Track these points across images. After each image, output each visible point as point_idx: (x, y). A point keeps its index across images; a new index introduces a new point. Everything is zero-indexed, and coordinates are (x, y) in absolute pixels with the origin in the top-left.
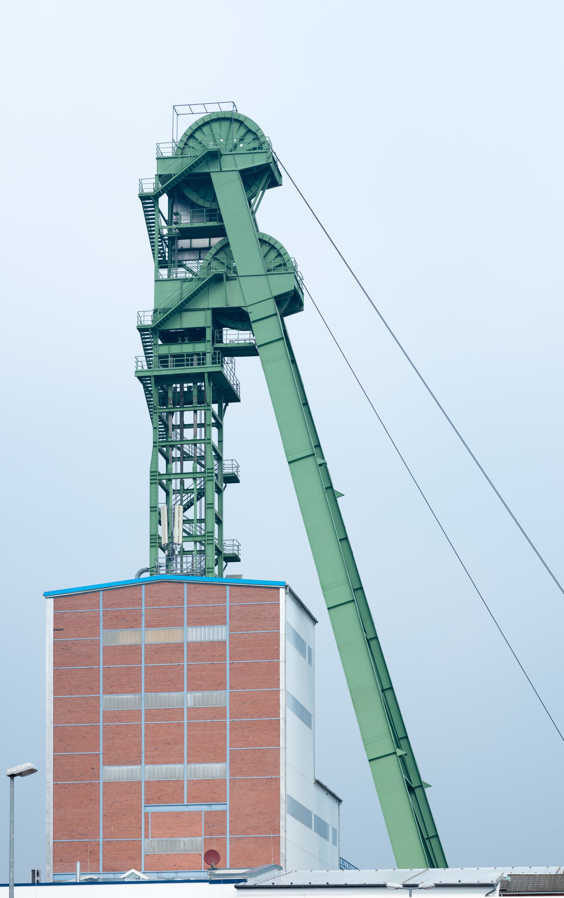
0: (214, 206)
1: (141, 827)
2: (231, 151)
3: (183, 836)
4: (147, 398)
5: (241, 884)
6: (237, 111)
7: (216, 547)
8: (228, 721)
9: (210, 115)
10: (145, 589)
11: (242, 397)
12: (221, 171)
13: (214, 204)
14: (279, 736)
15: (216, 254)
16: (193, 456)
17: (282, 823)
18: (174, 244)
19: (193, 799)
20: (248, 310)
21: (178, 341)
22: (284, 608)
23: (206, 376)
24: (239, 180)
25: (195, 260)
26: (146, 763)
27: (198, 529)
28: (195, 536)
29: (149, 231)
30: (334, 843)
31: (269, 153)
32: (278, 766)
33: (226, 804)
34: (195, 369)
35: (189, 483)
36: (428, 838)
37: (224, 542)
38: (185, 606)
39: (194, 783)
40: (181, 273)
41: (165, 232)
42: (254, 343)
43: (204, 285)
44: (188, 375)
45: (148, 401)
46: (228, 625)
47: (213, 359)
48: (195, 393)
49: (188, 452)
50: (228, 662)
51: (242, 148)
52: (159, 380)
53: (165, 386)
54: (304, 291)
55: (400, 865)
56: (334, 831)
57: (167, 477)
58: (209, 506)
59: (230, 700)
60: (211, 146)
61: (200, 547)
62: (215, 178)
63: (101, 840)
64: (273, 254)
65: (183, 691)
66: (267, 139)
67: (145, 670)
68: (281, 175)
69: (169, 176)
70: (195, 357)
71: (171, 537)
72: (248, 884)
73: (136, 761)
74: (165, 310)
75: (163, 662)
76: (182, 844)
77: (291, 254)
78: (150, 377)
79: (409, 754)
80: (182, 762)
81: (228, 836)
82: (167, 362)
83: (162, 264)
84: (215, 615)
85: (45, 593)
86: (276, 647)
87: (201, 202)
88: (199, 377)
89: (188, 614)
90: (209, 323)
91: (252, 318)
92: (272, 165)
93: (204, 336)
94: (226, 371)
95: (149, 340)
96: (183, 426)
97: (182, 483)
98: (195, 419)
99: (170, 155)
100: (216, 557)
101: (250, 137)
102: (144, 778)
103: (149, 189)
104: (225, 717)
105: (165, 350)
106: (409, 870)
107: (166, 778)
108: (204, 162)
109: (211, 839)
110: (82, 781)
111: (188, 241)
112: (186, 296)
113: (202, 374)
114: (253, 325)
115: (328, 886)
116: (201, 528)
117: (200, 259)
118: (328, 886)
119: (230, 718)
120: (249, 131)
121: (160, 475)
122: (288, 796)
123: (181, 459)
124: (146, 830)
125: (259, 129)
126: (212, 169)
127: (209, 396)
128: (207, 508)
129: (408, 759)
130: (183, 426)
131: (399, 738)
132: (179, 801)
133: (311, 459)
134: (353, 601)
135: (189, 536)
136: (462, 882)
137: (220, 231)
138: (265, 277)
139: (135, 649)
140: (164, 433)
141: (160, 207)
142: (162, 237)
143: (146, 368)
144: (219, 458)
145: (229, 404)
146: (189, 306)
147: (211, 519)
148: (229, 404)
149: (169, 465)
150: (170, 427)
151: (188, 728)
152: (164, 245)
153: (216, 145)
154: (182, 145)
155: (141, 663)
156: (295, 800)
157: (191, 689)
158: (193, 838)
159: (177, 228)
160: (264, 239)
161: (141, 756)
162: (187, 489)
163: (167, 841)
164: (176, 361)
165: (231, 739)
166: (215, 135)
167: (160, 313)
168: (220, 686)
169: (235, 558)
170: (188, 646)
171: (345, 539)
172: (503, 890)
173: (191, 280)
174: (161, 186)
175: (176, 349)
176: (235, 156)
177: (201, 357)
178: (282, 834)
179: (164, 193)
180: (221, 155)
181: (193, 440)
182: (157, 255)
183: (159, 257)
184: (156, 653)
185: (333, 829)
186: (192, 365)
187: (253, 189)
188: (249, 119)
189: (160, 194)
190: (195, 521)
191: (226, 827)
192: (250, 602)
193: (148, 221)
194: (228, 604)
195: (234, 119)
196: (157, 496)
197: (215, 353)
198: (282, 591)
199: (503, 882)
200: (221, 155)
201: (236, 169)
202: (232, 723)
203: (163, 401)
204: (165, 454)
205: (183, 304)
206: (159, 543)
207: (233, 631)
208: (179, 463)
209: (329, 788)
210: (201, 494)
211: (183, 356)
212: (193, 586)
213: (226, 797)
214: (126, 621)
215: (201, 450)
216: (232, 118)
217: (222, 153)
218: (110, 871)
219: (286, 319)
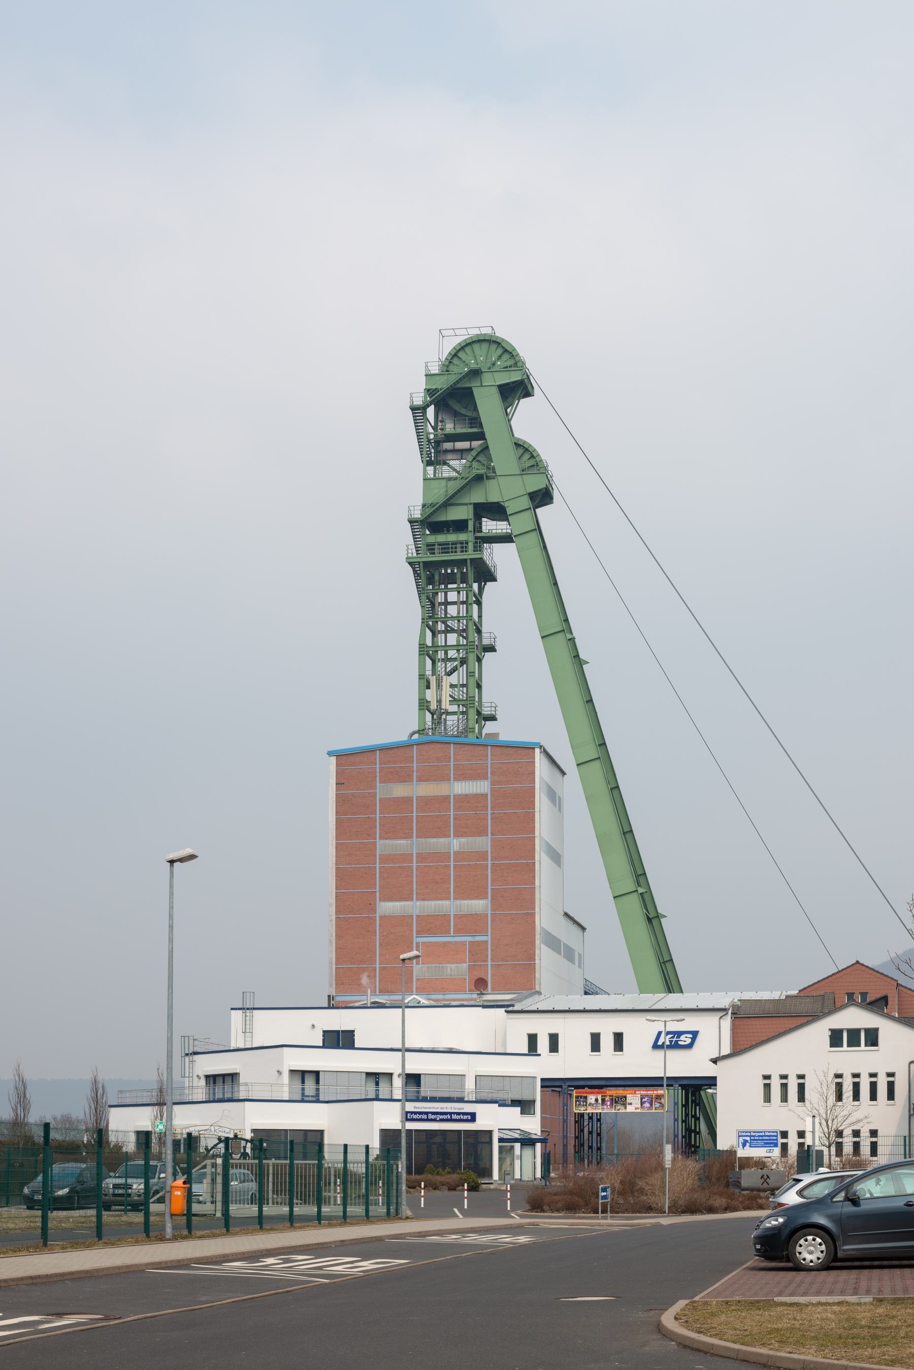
0: (475, 415)
2: (489, 368)
3: (449, 963)
4: (415, 580)
5: (510, 1009)
6: (495, 333)
7: (477, 709)
8: (490, 862)
9: (471, 337)
10: (417, 749)
11: (498, 577)
12: (482, 386)
13: (474, 413)
15: (476, 456)
16: (456, 629)
17: (537, 952)
18: (439, 446)
19: (459, 931)
20: (506, 504)
21: (443, 531)
22: (539, 765)
23: (469, 562)
24: (497, 394)
25: (457, 460)
26: (417, 900)
27: (461, 693)
28: (459, 700)
29: (418, 436)
30: (580, 966)
31: (524, 371)
32: (533, 903)
33: (488, 935)
34: (458, 556)
35: (452, 654)
36: (664, 962)
37: (483, 704)
38: (452, 763)
40: (446, 472)
41: (432, 436)
42: (510, 532)
43: (467, 484)
44: (452, 561)
45: (416, 583)
46: (489, 780)
47: (475, 547)
48: (459, 576)
49: (451, 625)
50: (489, 812)
51: (499, 365)
52: (427, 565)
53: (431, 570)
54: (554, 486)
55: (642, 991)
56: (580, 955)
57: (434, 649)
58: (470, 674)
59: (492, 845)
60: (473, 366)
61: (463, 709)
62: (476, 392)
63: (378, 966)
64: (527, 456)
65: (450, 837)
66: (522, 358)
67: (417, 819)
68: (533, 388)
69: (436, 390)
70: (459, 546)
71: (439, 702)
72: (515, 1008)
73: (409, 898)
74: (432, 505)
75: (432, 811)
76: (449, 970)
77: (543, 456)
78: (419, 562)
79: (649, 892)
80: (449, 899)
81: (489, 963)
82: (434, 549)
83: (429, 463)
84: (478, 772)
85: (328, 752)
86: (532, 799)
87: (463, 411)
88: (463, 562)
89: (454, 770)
90: (471, 516)
92: (525, 380)
93: (467, 527)
94: (486, 556)
95: (418, 530)
96: (447, 603)
97: (446, 653)
98: (459, 598)
99: (437, 372)
100: (477, 717)
101: (506, 356)
102: (416, 912)
103: (419, 401)
105: (432, 539)
106: (652, 995)
107: (435, 912)
110: (360, 914)
111: (452, 444)
112: (451, 492)
113: (466, 560)
114: (510, 518)
115: (585, 1011)
116: (463, 692)
117: (462, 459)
118: (585, 1011)
119: (491, 860)
120: (506, 351)
121: (427, 647)
122: (543, 928)
123: (445, 632)
125: (515, 349)
126: (474, 384)
127: (471, 576)
128: (470, 676)
129: (646, 896)
130: (447, 603)
132: (447, 932)
133: (561, 634)
134: (599, 758)
135: (454, 700)
136: (699, 1007)
137: (481, 436)
138: (520, 477)
139: (407, 800)
140: (430, 609)
141: (428, 416)
142: (429, 440)
143: (415, 555)
144: (479, 631)
145: (487, 583)
146: (452, 501)
147: (472, 684)
148: (487, 583)
149: (435, 639)
150: (437, 604)
151: (454, 869)
152: (431, 447)
153: (478, 364)
154: (447, 363)
155: (412, 813)
156: (548, 932)
157: (457, 835)
158: (458, 965)
159: (443, 434)
160: (519, 443)
161: (412, 894)
162: (451, 658)
163: (436, 967)
164: (442, 549)
166: (477, 356)
167: (428, 507)
168: (482, 832)
169: (493, 718)
170: (454, 798)
171: (590, 701)
172: (734, 1013)
173: (456, 479)
174: (429, 399)
175: (441, 538)
176: (494, 373)
177: (464, 545)
178: (537, 961)
179: (431, 404)
180: (482, 372)
181: (457, 617)
182: (425, 455)
183: (427, 457)
184: (426, 804)
185: (579, 954)
186: (456, 552)
187: (509, 400)
188: (506, 341)
189: (428, 406)
190: (459, 686)
191: (488, 955)
192: (508, 760)
193: (417, 428)
194: (489, 762)
195: (493, 341)
196: (425, 665)
197: (476, 543)
198: (537, 751)
199: (734, 1006)
200: (482, 372)
201: (495, 384)
202: (493, 865)
203: (430, 581)
204: (432, 628)
205: (448, 500)
206: (426, 706)
207: (494, 785)
208: (443, 635)
209: (576, 918)
210: (463, 661)
211: (449, 544)
212: (459, 746)
213: (487, 929)
214: (400, 776)
215: (463, 624)
216: (491, 340)
217: (483, 371)
218: (385, 993)
219: (537, 510)
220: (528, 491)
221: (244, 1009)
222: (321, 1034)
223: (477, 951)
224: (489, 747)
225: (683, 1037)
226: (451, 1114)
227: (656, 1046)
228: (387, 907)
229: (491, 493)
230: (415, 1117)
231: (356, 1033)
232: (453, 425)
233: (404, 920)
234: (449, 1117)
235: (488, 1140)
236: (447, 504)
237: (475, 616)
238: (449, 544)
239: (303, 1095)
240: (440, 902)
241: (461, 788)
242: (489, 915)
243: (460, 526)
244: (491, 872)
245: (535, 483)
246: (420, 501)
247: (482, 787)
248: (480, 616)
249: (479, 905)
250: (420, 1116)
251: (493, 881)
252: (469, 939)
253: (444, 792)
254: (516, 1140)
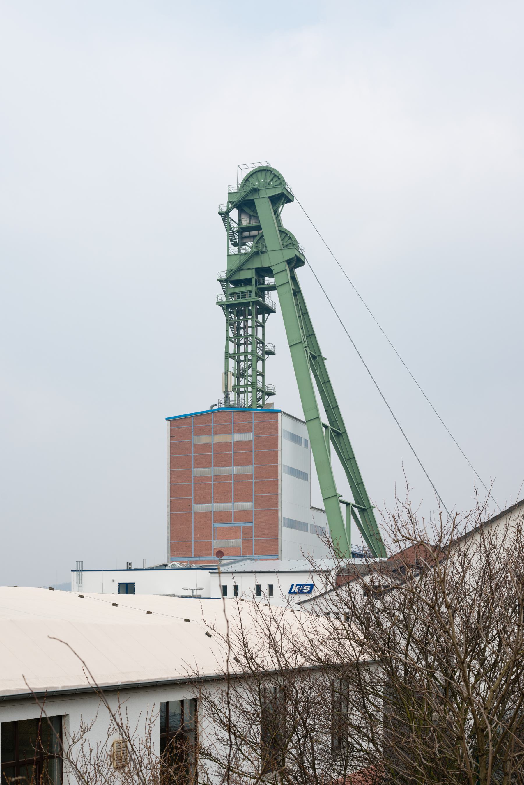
1: (212, 535)
2: (266, 187)
3: (232, 539)
8: (253, 481)
12: (259, 198)
14: (278, 488)
19: (237, 520)
20: (273, 268)
23: (251, 303)
26: (214, 503)
32: (277, 503)
38: (233, 423)
39: (237, 512)
46: (253, 432)
62: (256, 202)
63: (193, 541)
64: (287, 238)
73: (209, 502)
75: (222, 451)
76: (231, 543)
80: (231, 502)
81: (253, 539)
91: (274, 272)
99: (236, 191)
103: (225, 209)
104: (252, 479)
108: (251, 194)
109: (245, 540)
111: (249, 232)
112: (242, 261)
113: (249, 302)
120: (275, 175)
124: (214, 536)
126: (255, 197)
132: (230, 521)
133: (300, 345)
139: (208, 445)
146: (244, 267)
154: (242, 185)
155: (211, 452)
157: (236, 465)
158: (237, 540)
165: (255, 490)
168: (249, 463)
178: (279, 537)
180: (259, 190)
186: (245, 298)
187: (277, 205)
194: (253, 422)
198: (280, 414)
202: (255, 481)
211: (240, 293)
212: (237, 413)
221: (77, 571)
222: (118, 585)
223: (246, 532)
224: (253, 413)
227: (290, 592)
228: (198, 507)
229: (264, 262)
231: (135, 584)
232: (249, 221)
233: (206, 515)
236: (240, 269)
237: (260, 336)
238: (240, 293)
240: (227, 504)
241: (238, 437)
242: (253, 511)
243: (247, 282)
244: (255, 486)
245: (290, 254)
246: (225, 268)
247: (249, 437)
248: (264, 334)
249: (248, 505)
251: (255, 491)
252: (242, 525)
253: (229, 440)
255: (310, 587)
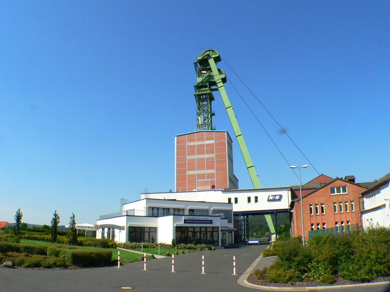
50: (215, 148)
52: (198, 95)
73: (194, 170)
124: (197, 185)
131: (152, 215)
139: (194, 146)
168: (213, 153)
220: (221, 78)
225: (276, 197)
226: (203, 220)
230: (189, 221)
234: (202, 222)
235: (155, 231)
239: (153, 214)
242: (215, 174)
247: (213, 142)
249: (213, 171)
250: (191, 221)
254: (227, 231)
255: (279, 196)
